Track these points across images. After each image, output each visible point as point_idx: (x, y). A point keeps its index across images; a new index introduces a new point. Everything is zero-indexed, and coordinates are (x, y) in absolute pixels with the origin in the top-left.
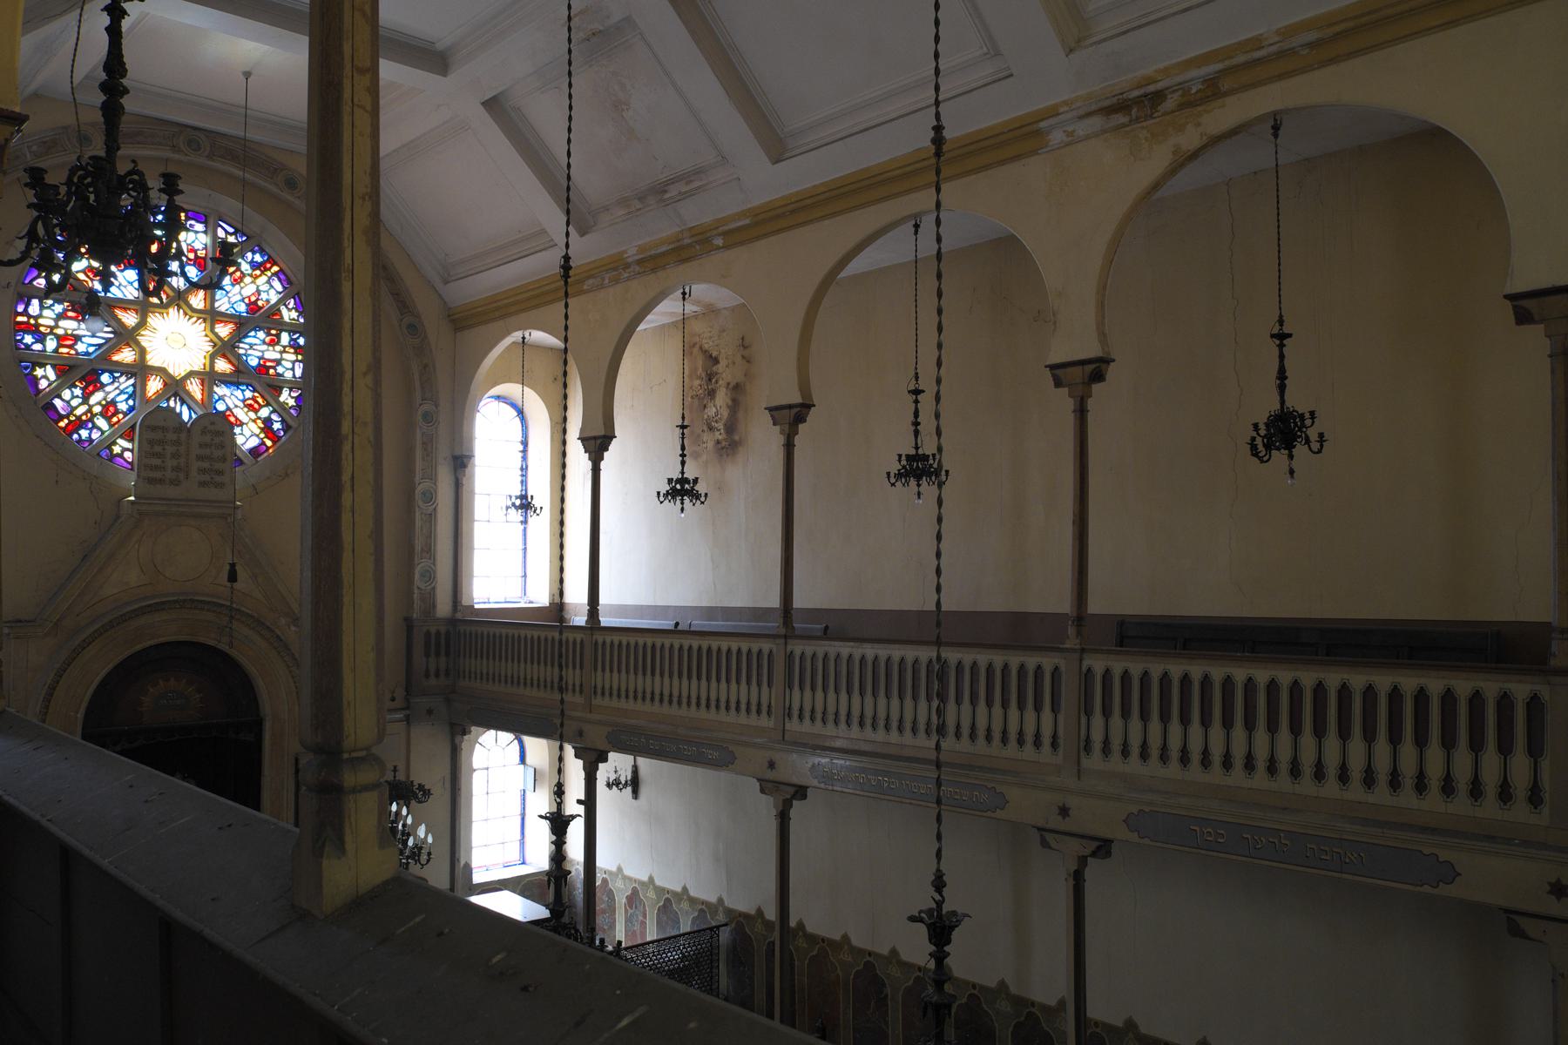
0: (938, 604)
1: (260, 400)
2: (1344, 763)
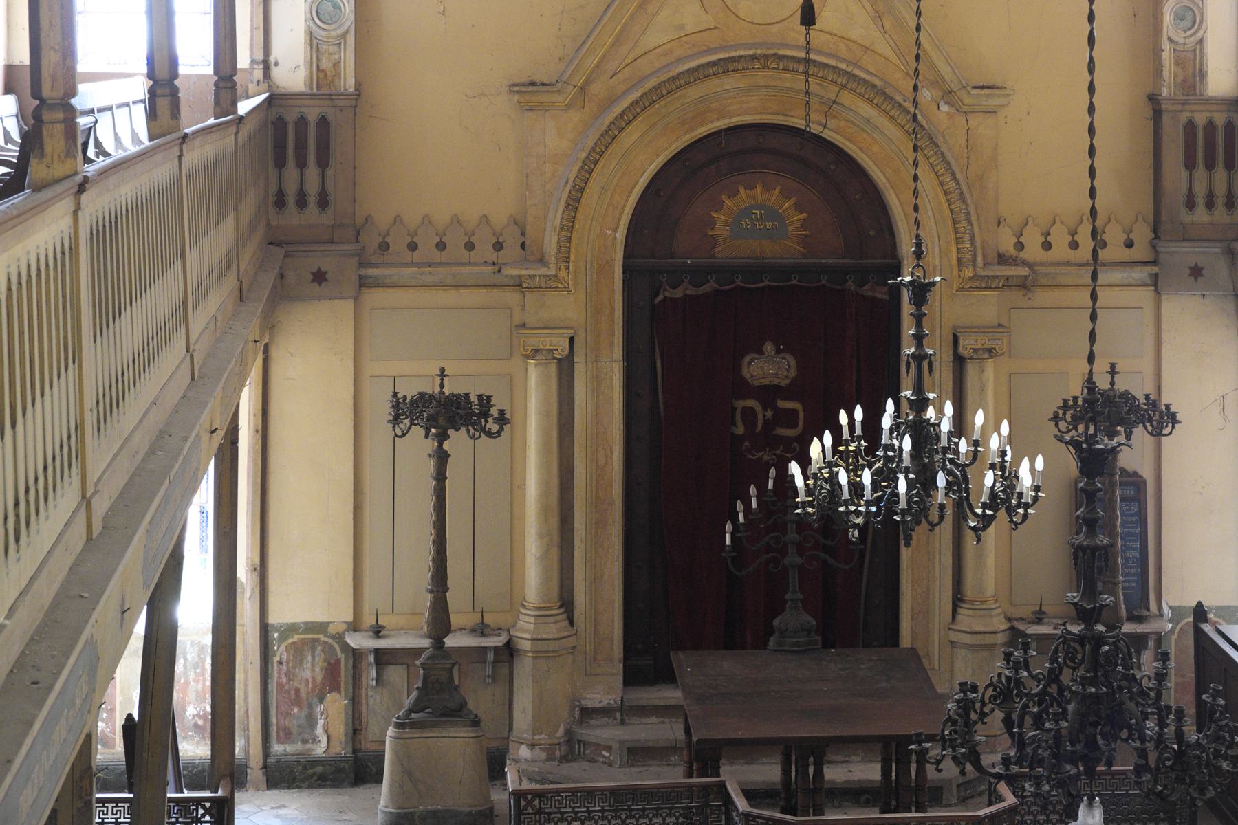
2: (301, 189)
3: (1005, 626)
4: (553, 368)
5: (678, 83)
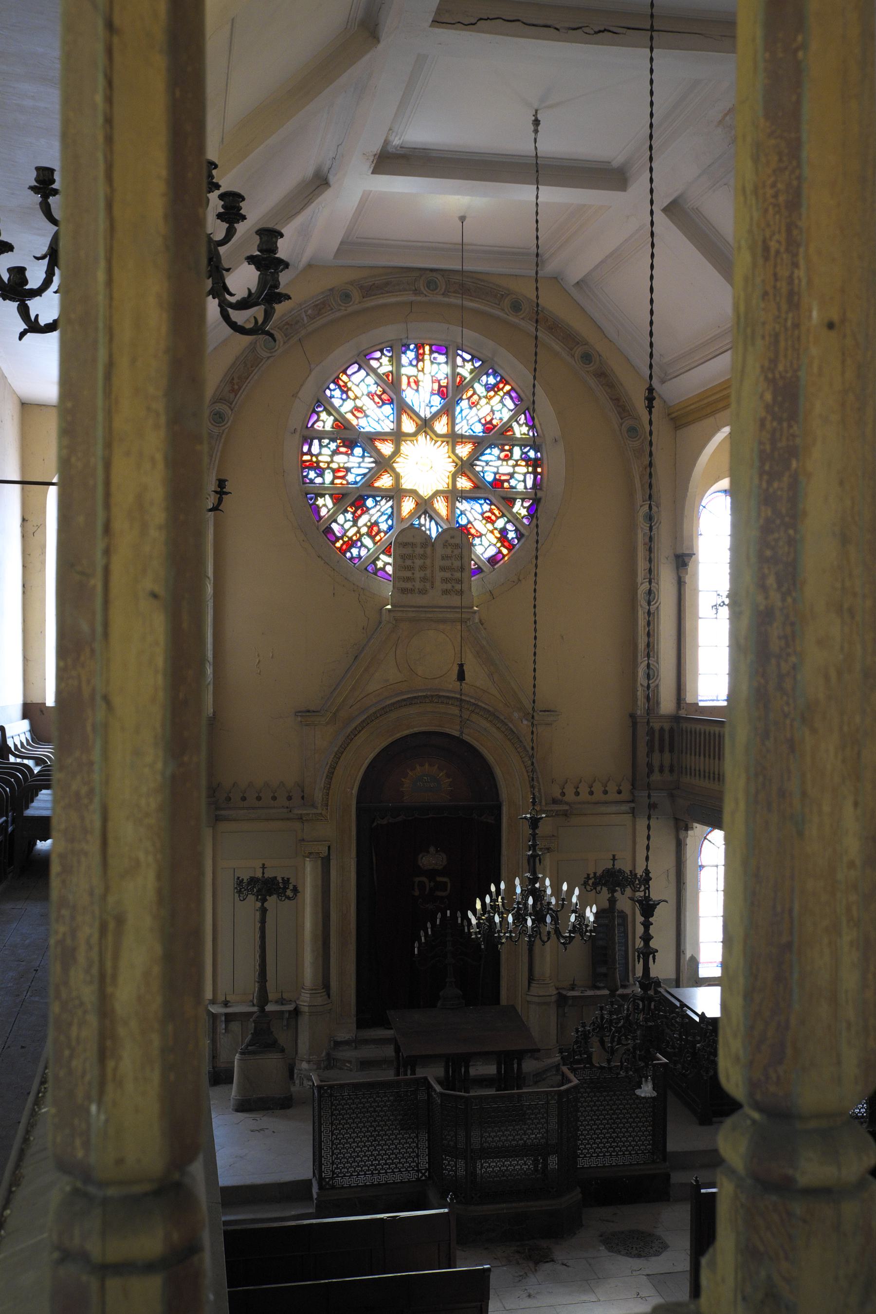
3: (555, 992)
4: (319, 862)
5: (385, 711)
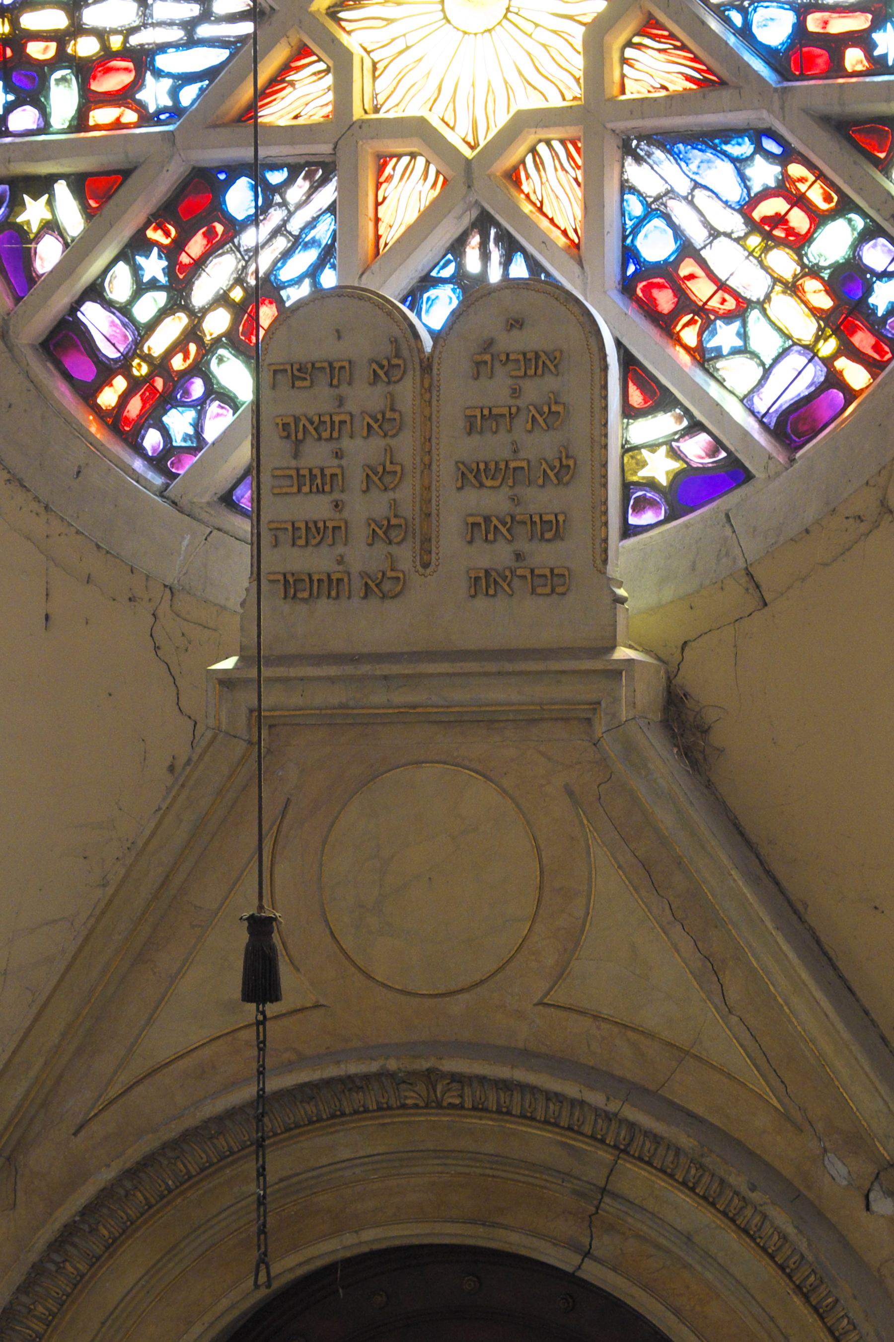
0: (583, 1260)
1: (816, 195)
